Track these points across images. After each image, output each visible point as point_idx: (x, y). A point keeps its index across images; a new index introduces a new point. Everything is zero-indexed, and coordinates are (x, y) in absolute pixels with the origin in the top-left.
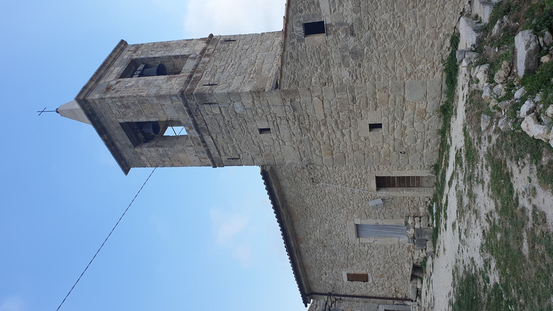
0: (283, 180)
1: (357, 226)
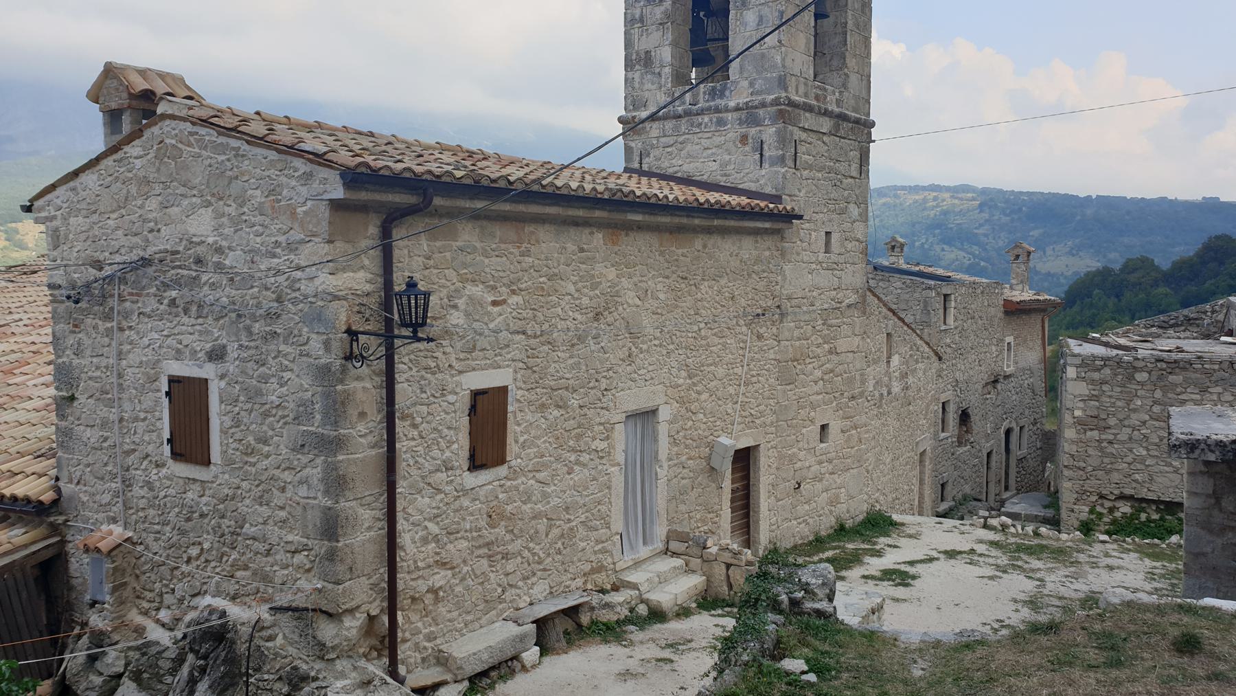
0: (756, 247)
1: (654, 412)
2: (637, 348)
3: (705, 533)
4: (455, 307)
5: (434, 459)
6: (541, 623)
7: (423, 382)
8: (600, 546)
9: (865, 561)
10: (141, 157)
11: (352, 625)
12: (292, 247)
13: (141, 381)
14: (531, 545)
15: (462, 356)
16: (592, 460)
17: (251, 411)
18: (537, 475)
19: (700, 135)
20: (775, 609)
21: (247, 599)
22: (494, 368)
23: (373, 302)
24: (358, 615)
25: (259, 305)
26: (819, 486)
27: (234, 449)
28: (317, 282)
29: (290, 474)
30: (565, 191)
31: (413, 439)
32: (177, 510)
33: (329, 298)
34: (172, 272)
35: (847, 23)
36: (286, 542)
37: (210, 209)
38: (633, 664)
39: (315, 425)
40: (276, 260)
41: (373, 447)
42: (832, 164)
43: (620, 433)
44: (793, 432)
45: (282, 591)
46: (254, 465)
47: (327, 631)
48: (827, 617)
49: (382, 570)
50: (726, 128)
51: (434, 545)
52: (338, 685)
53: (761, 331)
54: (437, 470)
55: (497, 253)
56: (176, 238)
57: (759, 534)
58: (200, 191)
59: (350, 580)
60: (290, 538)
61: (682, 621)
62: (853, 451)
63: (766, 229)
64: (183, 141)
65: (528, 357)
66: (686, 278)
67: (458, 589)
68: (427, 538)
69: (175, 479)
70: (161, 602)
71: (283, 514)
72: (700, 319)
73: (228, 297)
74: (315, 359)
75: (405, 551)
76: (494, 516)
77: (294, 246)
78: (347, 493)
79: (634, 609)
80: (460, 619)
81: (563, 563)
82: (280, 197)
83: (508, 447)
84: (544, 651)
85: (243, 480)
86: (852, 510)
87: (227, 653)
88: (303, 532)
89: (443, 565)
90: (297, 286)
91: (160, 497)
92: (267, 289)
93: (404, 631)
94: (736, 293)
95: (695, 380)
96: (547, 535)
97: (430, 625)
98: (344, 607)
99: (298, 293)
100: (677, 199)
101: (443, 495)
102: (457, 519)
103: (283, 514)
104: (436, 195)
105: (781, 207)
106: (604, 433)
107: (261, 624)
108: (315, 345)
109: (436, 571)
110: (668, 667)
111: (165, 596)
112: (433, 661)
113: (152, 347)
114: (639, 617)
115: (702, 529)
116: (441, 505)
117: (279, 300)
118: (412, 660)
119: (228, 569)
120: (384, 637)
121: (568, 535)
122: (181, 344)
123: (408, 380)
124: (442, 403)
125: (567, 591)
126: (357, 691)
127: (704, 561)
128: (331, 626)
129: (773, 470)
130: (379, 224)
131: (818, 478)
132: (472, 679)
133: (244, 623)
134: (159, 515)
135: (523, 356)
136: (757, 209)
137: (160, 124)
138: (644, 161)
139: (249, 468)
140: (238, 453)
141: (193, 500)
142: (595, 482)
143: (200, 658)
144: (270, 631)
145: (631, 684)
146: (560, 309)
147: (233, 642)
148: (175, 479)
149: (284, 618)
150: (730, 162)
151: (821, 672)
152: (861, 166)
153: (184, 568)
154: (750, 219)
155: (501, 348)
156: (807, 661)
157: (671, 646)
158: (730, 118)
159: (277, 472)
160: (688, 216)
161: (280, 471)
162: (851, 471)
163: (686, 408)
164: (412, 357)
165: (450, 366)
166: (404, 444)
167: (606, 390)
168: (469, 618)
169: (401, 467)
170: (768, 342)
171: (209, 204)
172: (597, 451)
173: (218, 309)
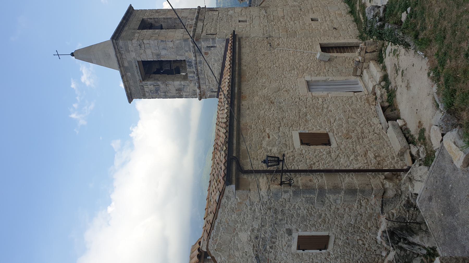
2: (284, 89)
3: (354, 62)
4: (271, 150)
5: (326, 157)
6: (388, 119)
7: (298, 161)
8: (359, 100)
9: (364, 2)
10: (221, 258)
11: (388, 184)
12: (252, 204)
13: (299, 260)
14: (358, 124)
15: (288, 148)
16: (326, 103)
17: (310, 220)
18: (332, 122)
19: (205, 70)
20: (383, 27)
21: (378, 223)
22: (292, 137)
23: (270, 177)
24: (384, 183)
25: (272, 216)
26: (335, 21)
27: (323, 227)
28: (264, 195)
29: (332, 206)
30: (229, 114)
31: (319, 164)
32: (345, 248)
33: (269, 191)
34: (260, 247)
35: (163, 18)
36: (357, 208)
37: (239, 233)
38: (404, 85)
39: (315, 197)
40: (256, 210)
41: (322, 177)
42: (214, 21)
43: (315, 94)
44: (314, 31)
45: (375, 210)
46: (329, 220)
47: (391, 193)
48: (386, 7)
49: (368, 175)
50: (202, 61)
51: (358, 157)
52: (411, 189)
53: (276, 44)
54: (331, 156)
55: (251, 137)
56: (248, 246)
57: (354, 43)
58: (232, 237)
59: (371, 185)
60: (356, 207)
61: (388, 69)
62: (321, 9)
63: (238, 44)
64: (215, 242)
65: (288, 126)
66: (257, 72)
67: (375, 149)
68: (356, 159)
69: (334, 249)
70: (379, 255)
71: (347, 209)
72: (272, 66)
73: (269, 227)
74: (291, 196)
75: (360, 167)
76: (348, 137)
77: (251, 203)
78: (339, 186)
79: (383, 87)
80: (386, 148)
81: (365, 113)
82: (235, 208)
83: (322, 132)
84: (399, 118)
85: (335, 224)
86: (344, 9)
87: (398, 230)
88: (354, 202)
89: (366, 154)
90: (265, 202)
91: (341, 254)
92: (266, 213)
93: (391, 167)
94: (262, 54)
95: (295, 68)
96: (355, 119)
97: (388, 158)
98: (381, 187)
99: (267, 202)
100: (229, 75)
101: (340, 154)
102: (349, 150)
103: (347, 209)
104: (232, 155)
105: (230, 39)
106: (316, 100)
107: (388, 218)
108: (286, 196)
109: (368, 156)
110: (405, 72)
111: (377, 253)
112: (402, 157)
113: (287, 256)
114: (386, 85)
115: (352, 64)
116: (343, 155)
117: (270, 209)
118: (402, 164)
119: (367, 230)
120: (393, 174)
121: (355, 111)
122: (286, 245)
123: (298, 166)
124: (306, 155)
125: (376, 111)
126: (413, 183)
127: (364, 62)
128: (388, 192)
129: (329, 38)
130: (243, 175)
131: (332, 21)
132: (409, 143)
133: (387, 224)
134: (347, 255)
135: (288, 128)
136: (232, 47)
137: (210, 250)
138: (214, 91)
139: (330, 221)
140: (325, 225)
141: (342, 242)
142: (335, 102)
143: (400, 240)
144: (390, 215)
145: (411, 85)
146: (270, 116)
147: (394, 228)
148: (334, 249)
149: (385, 209)
150: (214, 59)
151: (407, 6)
152: (214, 11)
153: (367, 246)
154: (235, 49)
155: (285, 135)
156: (403, 12)
157: (397, 72)
158: (199, 59)
159: (332, 211)
160: (235, 72)
161: (331, 210)
162: (329, 9)
163: (306, 70)
164: (289, 164)
165: (292, 152)
166: (321, 167)
167: (299, 99)
168: (386, 145)
169: (329, 168)
170: (280, 42)
171: (237, 233)
172: (323, 101)
173: (273, 231)
